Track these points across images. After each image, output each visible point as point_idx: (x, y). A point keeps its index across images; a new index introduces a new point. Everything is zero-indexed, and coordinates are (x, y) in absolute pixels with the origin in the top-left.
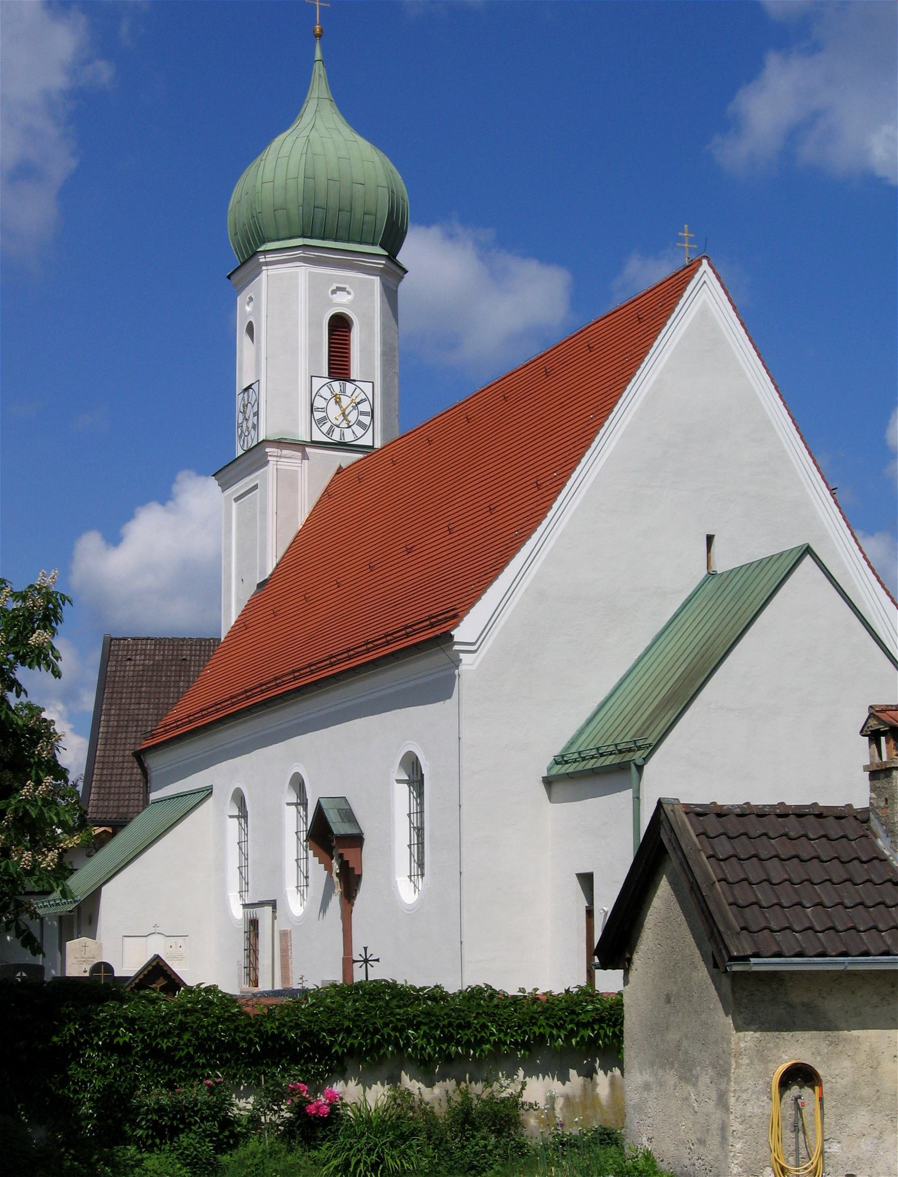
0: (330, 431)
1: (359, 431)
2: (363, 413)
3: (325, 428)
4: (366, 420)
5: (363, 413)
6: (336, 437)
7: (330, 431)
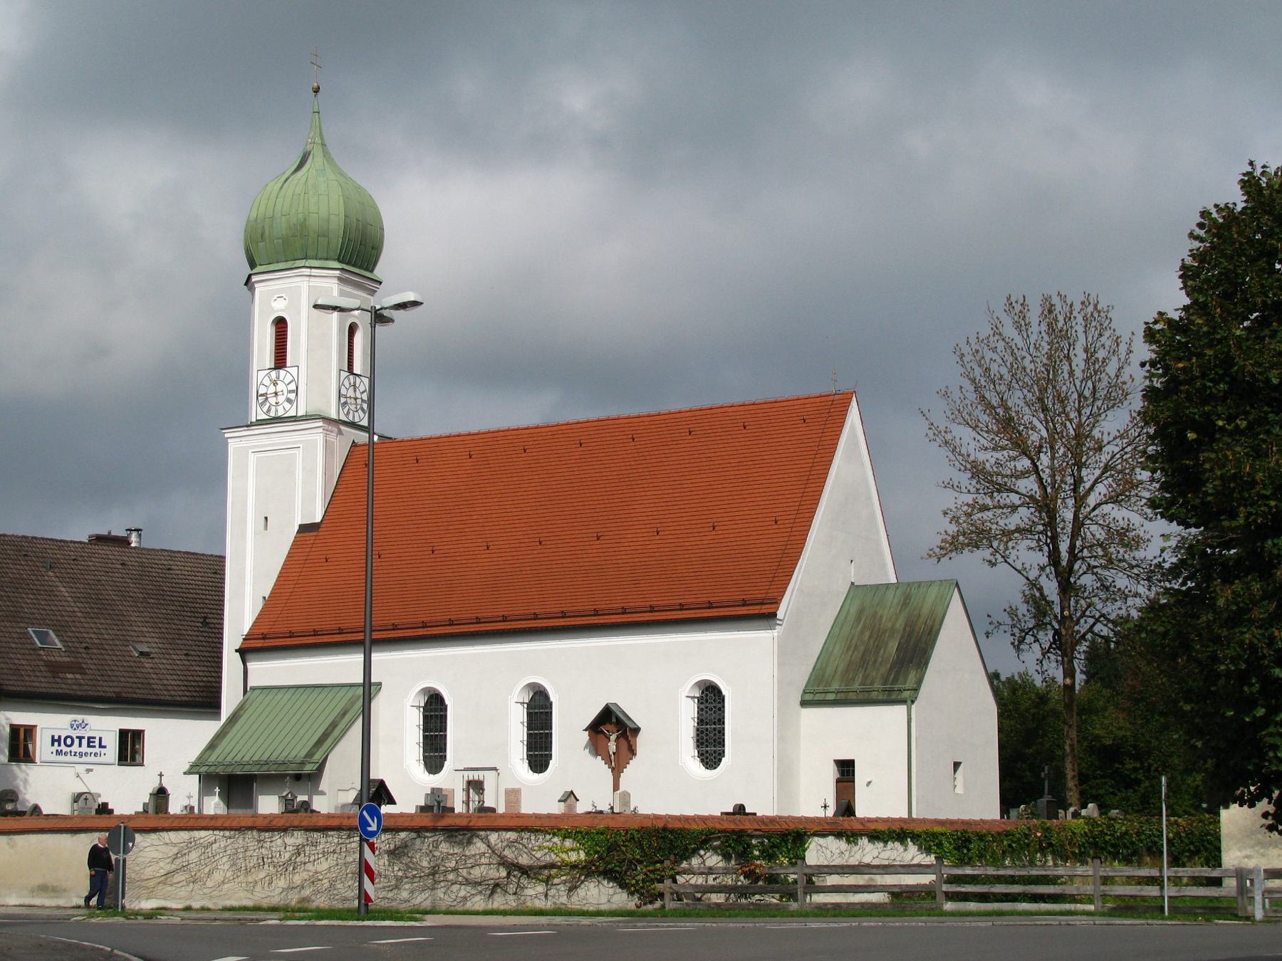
0: (269, 410)
1: (287, 405)
2: (290, 392)
3: (265, 409)
4: (292, 396)
5: (290, 392)
6: (272, 414)
7: (269, 410)
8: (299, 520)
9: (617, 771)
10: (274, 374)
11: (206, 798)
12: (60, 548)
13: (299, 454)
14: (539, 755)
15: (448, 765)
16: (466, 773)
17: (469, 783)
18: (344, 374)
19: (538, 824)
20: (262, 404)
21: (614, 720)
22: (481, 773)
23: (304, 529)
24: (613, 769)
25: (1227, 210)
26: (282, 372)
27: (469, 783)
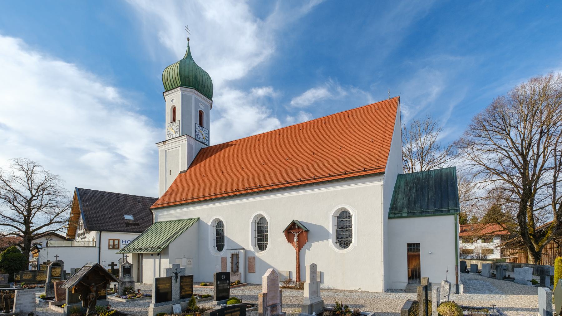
8: (180, 170)
9: (300, 247)
10: (172, 124)
11: (97, 262)
12: (139, 202)
13: (180, 148)
14: (262, 241)
15: (225, 248)
16: (231, 251)
17: (233, 255)
18: (197, 125)
19: (429, 308)
20: (168, 135)
21: (296, 227)
22: (237, 251)
23: (181, 172)
24: (191, 58)
25: (322, 281)
26: (174, 123)
27: (233, 255)
